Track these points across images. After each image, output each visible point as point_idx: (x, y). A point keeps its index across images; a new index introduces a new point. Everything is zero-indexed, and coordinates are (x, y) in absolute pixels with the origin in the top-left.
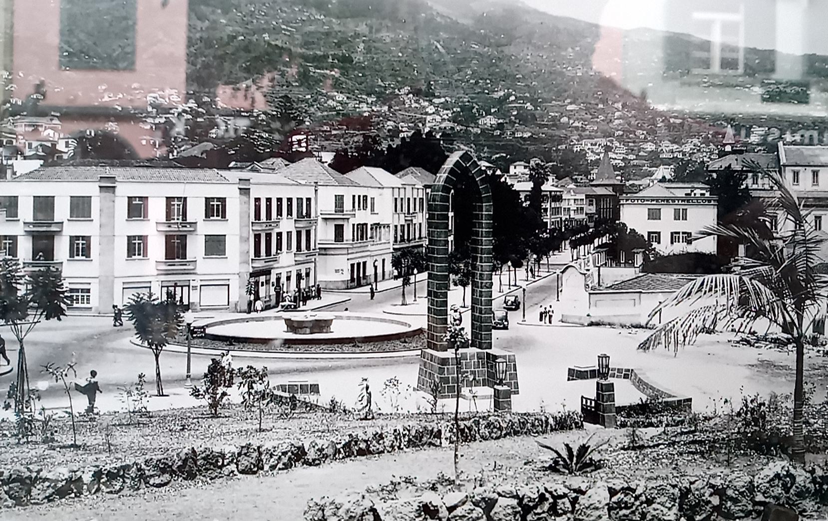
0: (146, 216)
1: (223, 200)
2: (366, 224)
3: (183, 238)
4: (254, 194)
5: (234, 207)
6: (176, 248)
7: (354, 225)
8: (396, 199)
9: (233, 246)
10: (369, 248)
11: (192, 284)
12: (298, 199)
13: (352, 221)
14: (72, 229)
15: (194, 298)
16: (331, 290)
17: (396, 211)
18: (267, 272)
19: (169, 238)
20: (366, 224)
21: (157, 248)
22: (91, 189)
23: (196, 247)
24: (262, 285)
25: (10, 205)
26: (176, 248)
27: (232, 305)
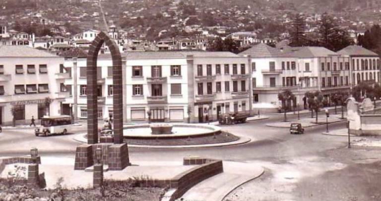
0: (142, 75)
1: (179, 66)
2: (295, 77)
3: (160, 85)
4: (197, 62)
5: (184, 71)
6: (157, 90)
7: (284, 78)
8: (323, 64)
9: (185, 89)
10: (299, 90)
11: (165, 108)
12: (292, 62)
13: (282, 76)
14: (171, 81)
15: (167, 116)
16: (262, 114)
17: (323, 69)
18: (210, 103)
19: (153, 86)
20: (295, 77)
21: (147, 91)
22: (182, 62)
23: (167, 90)
24: (240, 106)
25: (38, 134)
26: (157, 90)
27: (169, 112)
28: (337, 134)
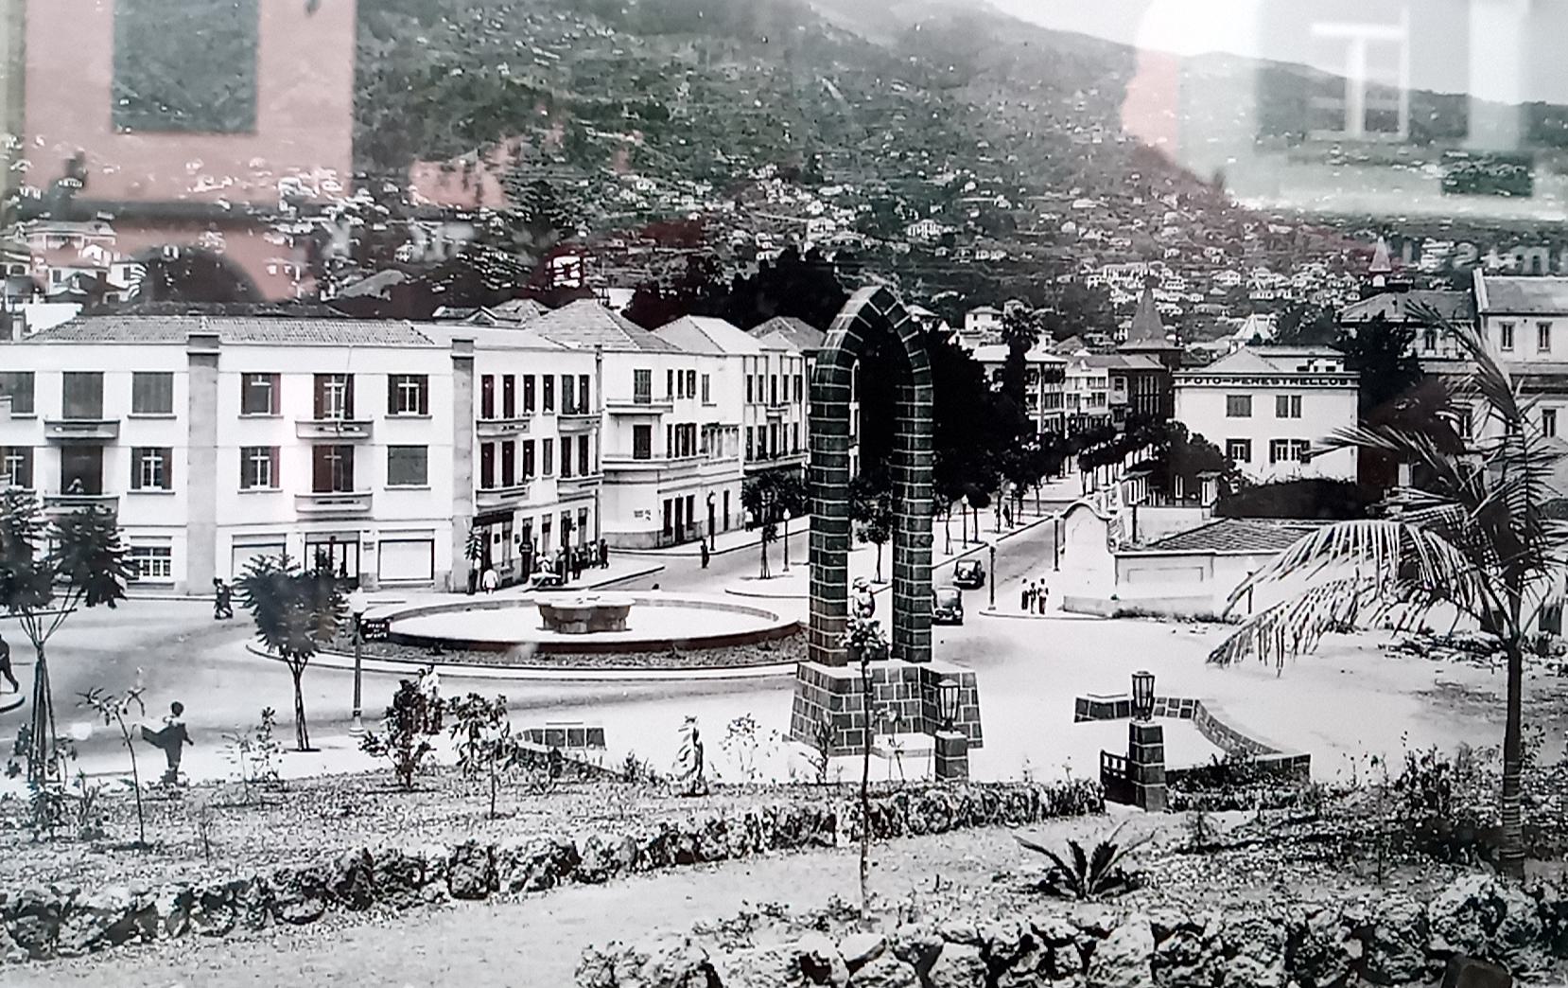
0: (276, 409)
1: (422, 380)
2: (694, 425)
3: (347, 452)
4: (480, 368)
5: (443, 392)
6: (333, 470)
7: (669, 427)
8: (750, 378)
9: (440, 466)
10: (699, 470)
11: (364, 538)
12: (564, 377)
13: (667, 419)
15: (368, 565)
16: (626, 551)
17: (750, 399)
18: (506, 516)
19: (319, 452)
20: (694, 425)
21: (297, 470)
22: (172, 359)
23: (370, 469)
24: (497, 541)
26: (333, 470)
28: (1143, 357)
